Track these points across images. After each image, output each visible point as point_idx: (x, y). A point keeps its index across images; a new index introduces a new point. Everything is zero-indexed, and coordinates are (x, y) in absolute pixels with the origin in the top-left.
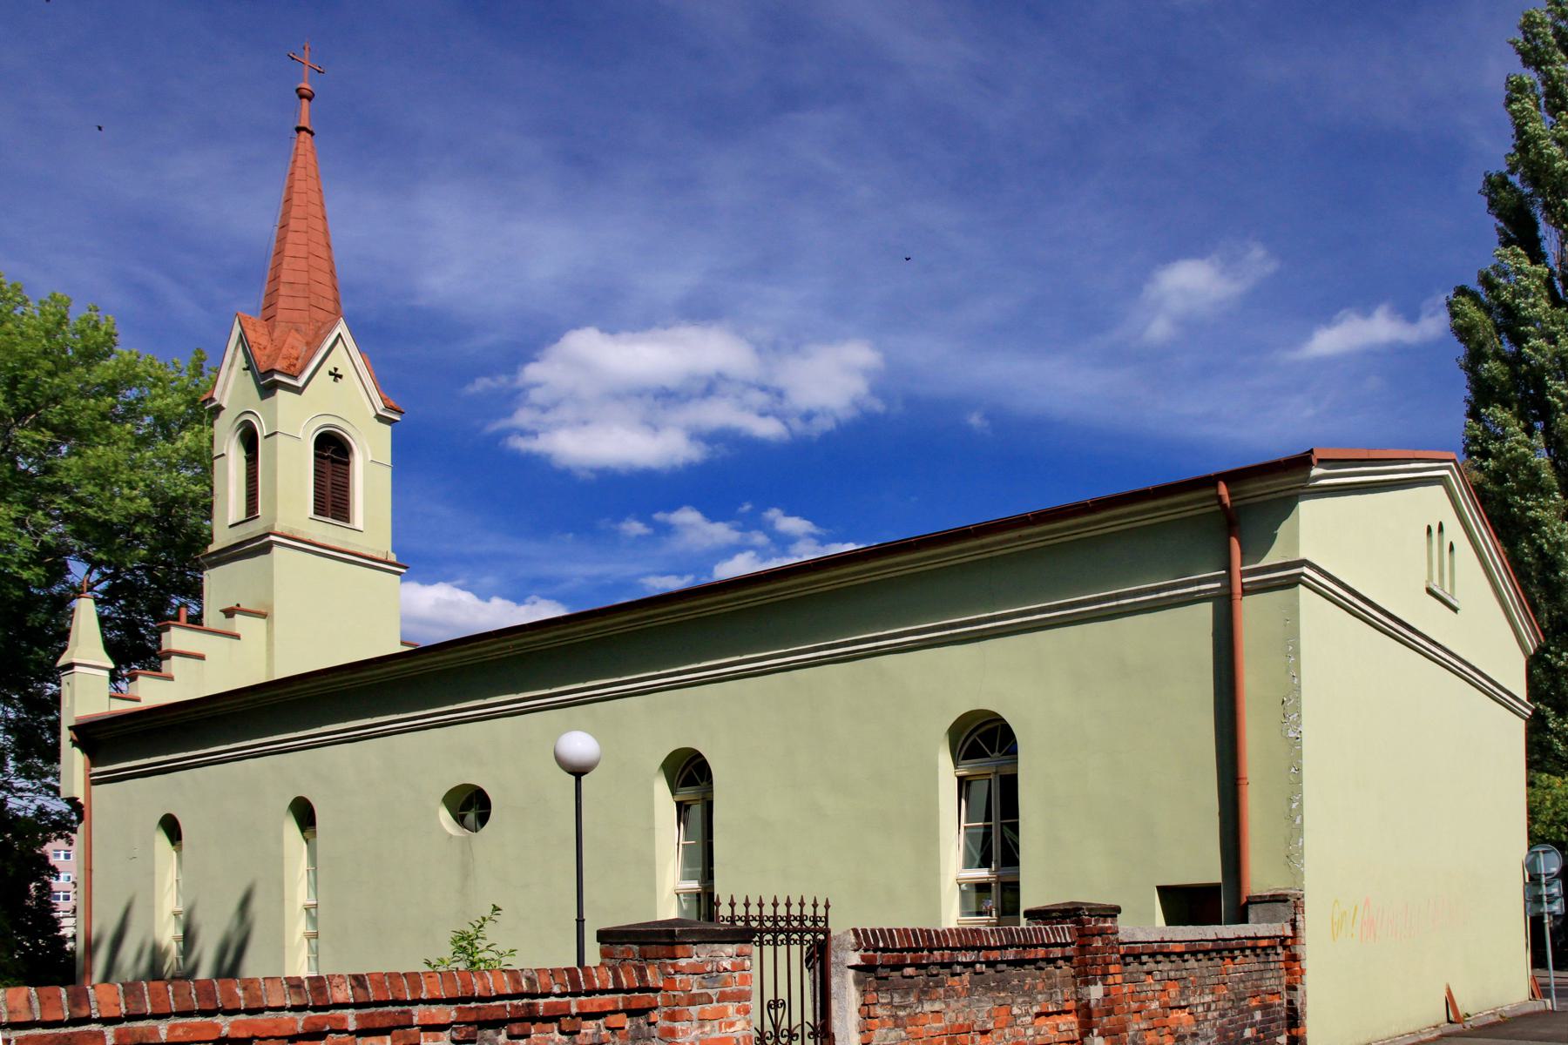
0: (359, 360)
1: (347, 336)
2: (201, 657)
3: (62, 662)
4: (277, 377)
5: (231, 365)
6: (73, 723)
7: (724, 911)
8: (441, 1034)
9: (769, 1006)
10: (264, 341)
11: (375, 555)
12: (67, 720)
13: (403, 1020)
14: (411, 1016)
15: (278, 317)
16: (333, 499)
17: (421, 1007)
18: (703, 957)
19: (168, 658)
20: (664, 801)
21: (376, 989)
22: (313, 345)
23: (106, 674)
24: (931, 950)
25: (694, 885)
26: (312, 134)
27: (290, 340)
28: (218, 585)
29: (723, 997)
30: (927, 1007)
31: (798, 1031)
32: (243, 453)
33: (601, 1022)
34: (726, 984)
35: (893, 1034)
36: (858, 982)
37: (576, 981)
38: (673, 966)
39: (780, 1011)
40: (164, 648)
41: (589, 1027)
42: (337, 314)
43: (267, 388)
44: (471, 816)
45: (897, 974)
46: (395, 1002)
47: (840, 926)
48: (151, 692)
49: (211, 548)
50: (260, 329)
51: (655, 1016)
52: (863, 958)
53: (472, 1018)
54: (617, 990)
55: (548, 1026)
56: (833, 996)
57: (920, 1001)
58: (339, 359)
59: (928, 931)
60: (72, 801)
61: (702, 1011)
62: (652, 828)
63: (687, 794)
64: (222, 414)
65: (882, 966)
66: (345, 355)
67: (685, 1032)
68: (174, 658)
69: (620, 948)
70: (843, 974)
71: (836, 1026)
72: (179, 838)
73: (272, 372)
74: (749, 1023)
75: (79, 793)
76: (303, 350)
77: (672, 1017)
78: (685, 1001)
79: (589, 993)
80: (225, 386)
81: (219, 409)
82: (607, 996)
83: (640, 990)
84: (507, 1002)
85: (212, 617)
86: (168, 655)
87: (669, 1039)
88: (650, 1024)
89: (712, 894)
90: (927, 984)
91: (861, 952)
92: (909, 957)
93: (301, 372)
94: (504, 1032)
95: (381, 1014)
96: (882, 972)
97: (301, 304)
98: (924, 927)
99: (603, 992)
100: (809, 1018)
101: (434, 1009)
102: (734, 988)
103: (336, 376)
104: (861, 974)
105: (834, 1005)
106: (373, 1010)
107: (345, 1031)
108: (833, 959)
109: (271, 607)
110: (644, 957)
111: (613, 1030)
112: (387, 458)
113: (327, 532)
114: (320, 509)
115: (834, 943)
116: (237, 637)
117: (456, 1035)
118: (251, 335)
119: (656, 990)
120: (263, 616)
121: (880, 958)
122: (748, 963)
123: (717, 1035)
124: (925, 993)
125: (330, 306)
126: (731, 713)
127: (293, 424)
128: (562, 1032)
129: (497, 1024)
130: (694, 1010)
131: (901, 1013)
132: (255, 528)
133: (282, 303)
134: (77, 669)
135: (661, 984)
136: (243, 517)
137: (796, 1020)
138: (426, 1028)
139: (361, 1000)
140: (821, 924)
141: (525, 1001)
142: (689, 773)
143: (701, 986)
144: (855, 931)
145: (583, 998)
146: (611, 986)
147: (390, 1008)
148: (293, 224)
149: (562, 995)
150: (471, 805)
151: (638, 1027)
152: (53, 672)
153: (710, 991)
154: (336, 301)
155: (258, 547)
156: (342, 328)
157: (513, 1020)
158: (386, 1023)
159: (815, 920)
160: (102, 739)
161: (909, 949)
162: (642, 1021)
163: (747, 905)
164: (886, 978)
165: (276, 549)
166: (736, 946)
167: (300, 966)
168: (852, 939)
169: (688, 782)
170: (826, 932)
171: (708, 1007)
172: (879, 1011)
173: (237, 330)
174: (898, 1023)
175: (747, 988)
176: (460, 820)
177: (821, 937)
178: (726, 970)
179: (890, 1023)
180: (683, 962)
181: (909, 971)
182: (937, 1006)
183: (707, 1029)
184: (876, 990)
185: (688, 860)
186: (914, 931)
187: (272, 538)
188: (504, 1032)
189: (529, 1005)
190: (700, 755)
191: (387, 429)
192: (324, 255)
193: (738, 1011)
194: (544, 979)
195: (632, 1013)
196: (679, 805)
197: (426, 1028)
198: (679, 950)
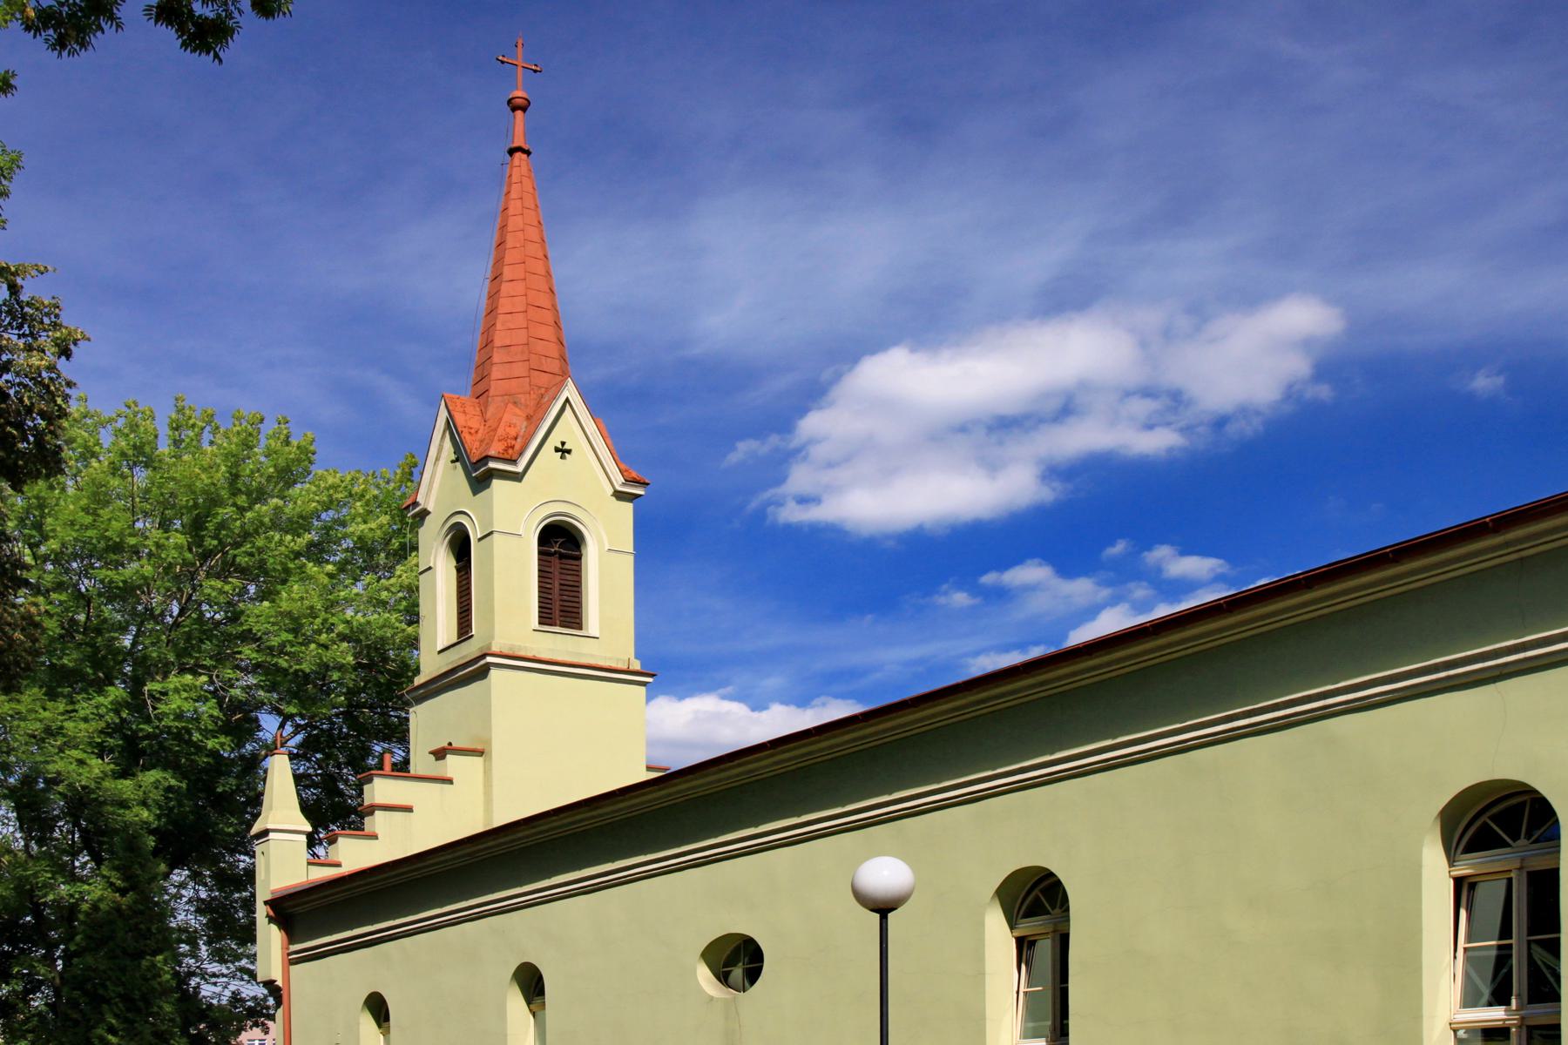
0: (591, 427)
2: (409, 809)
3: (255, 830)
4: (492, 465)
5: (437, 459)
6: (269, 897)
10: (475, 423)
11: (614, 665)
15: (492, 392)
16: (561, 605)
19: (372, 813)
20: (999, 937)
22: (533, 420)
23: (303, 838)
26: (528, 153)
27: (506, 417)
28: (427, 723)
40: (366, 803)
43: (480, 480)
49: (418, 681)
60: (270, 984)
63: (1028, 927)
66: (575, 425)
72: (387, 1019)
73: (486, 458)
75: (277, 976)
76: (522, 425)
85: (420, 761)
86: (372, 809)
93: (521, 453)
97: (520, 369)
103: (563, 451)
109: (489, 742)
113: (556, 644)
114: (546, 618)
116: (450, 781)
118: (460, 419)
125: (554, 366)
127: (511, 519)
132: (469, 650)
133: (496, 373)
134: (272, 835)
142: (1036, 900)
148: (507, 273)
150: (738, 960)
154: (563, 358)
155: (474, 672)
156: (570, 391)
160: (313, 914)
165: (494, 672)
169: (1033, 911)
173: (443, 415)
176: (723, 978)
187: (489, 659)
191: (628, 508)
196: (1020, 942)
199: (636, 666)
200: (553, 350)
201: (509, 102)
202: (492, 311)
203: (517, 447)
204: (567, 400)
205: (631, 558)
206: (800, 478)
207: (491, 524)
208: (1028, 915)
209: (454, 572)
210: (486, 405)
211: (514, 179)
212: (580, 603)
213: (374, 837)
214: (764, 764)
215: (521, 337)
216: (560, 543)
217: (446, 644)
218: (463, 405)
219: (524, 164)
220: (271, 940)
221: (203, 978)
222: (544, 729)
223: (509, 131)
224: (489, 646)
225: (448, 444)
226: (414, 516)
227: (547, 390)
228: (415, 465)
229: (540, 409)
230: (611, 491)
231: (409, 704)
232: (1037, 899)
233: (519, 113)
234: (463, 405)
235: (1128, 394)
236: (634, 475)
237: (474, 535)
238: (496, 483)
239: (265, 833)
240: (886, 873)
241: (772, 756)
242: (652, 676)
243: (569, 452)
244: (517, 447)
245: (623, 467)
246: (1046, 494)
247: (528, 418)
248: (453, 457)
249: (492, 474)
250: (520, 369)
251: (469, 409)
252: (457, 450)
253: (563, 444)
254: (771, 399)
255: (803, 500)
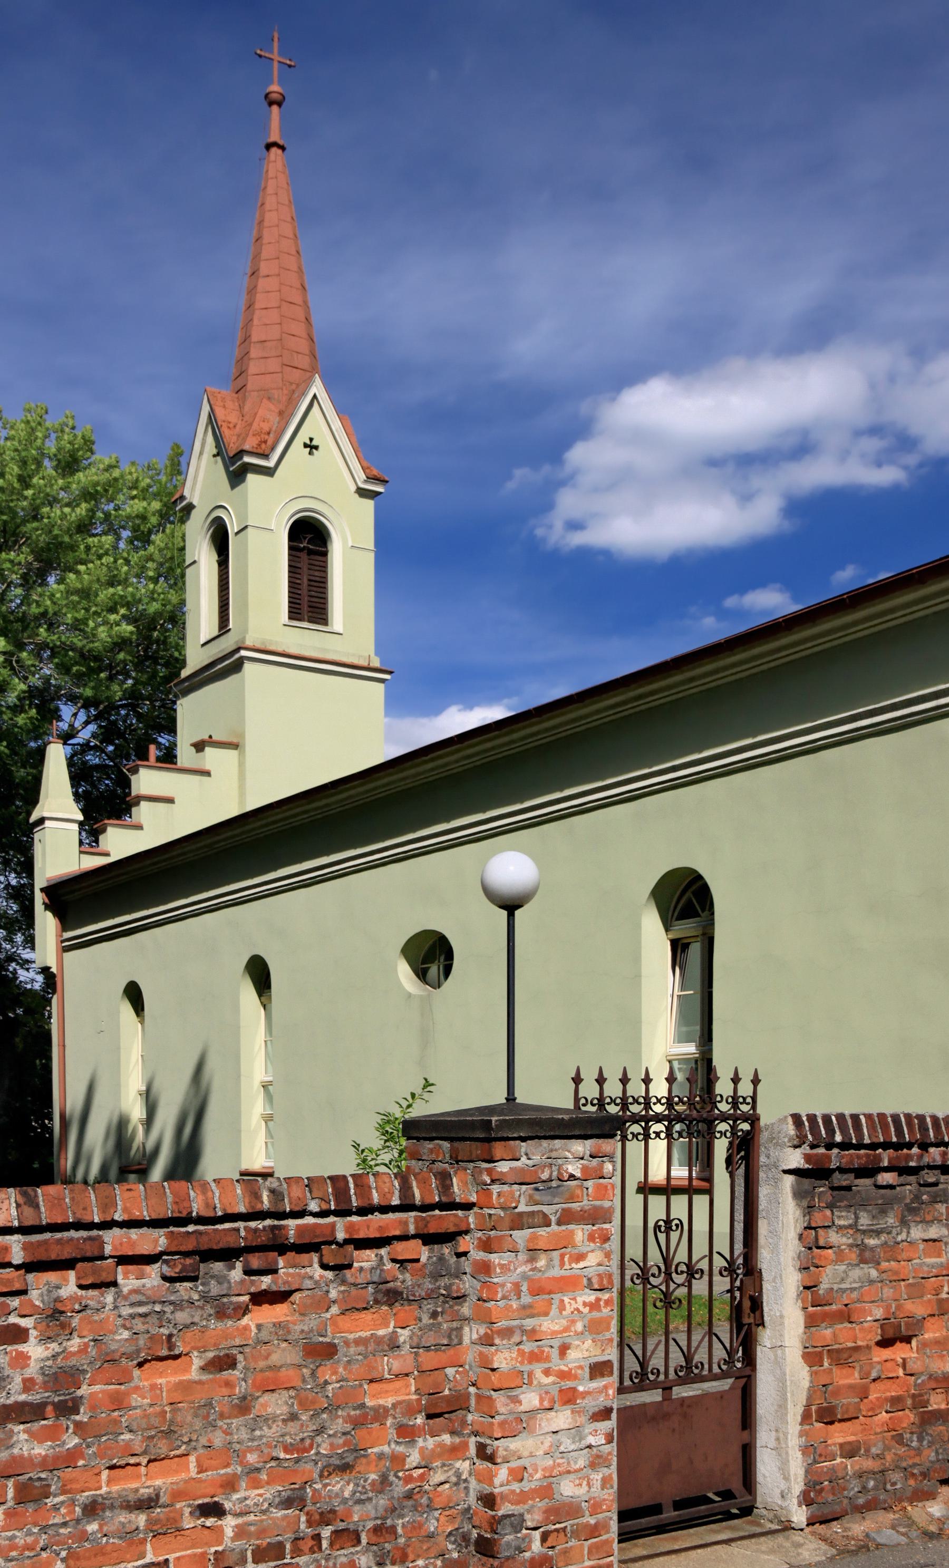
0: (336, 424)
1: (323, 396)
2: (170, 801)
3: (33, 818)
4: (247, 459)
5: (201, 453)
6: (44, 884)
7: (723, 1088)
8: (148, 1269)
9: (657, 1227)
10: (233, 418)
11: (356, 661)
12: (40, 882)
13: (89, 1251)
14: (102, 1244)
15: (249, 387)
16: (309, 600)
17: (116, 1231)
18: (537, 1158)
19: (137, 804)
20: (654, 938)
21: (50, 1209)
22: (285, 415)
23: (75, 827)
24: (924, 1146)
25: (691, 1049)
26: (283, 148)
27: (261, 413)
28: (193, 714)
29: (566, 1218)
30: (917, 1233)
31: (704, 1265)
32: (216, 557)
33: (383, 1251)
34: (572, 1198)
35: (856, 1273)
36: (798, 1194)
37: (342, 1197)
38: (490, 1172)
39: (674, 1236)
40: (133, 794)
41: (366, 1259)
42: (313, 370)
43: (237, 476)
44: (433, 970)
45: (867, 1182)
46: (78, 1225)
47: (773, 1112)
48: (120, 843)
49: (185, 673)
50: (229, 404)
51: (466, 1243)
52: (807, 1158)
53: (189, 1246)
54: (405, 1207)
55: (304, 1258)
56: (762, 1214)
57: (904, 1223)
58: (315, 427)
59: (921, 1118)
60: (45, 970)
61: (534, 1238)
62: (638, 976)
63: (685, 928)
64: (194, 513)
65: (841, 1170)
66: (322, 421)
67: (505, 1268)
68: (143, 803)
69: (429, 1145)
70: (777, 1181)
71: (765, 1258)
72: (143, 1009)
73: (241, 453)
74: (608, 1255)
75: (52, 963)
76: (274, 420)
77: (487, 1246)
78: (507, 1223)
79: (363, 1211)
80: (196, 477)
81: (190, 508)
82: (390, 1216)
83: (442, 1206)
84: (240, 1225)
85: (185, 754)
86: (139, 799)
87: (483, 1278)
88: (459, 1255)
89: (710, 1061)
90: (917, 1198)
91: (806, 1149)
92: (886, 1157)
93: (273, 448)
94: (239, 1265)
95: (59, 1241)
96: (839, 1179)
97: (273, 365)
98: (914, 1110)
99: (385, 1209)
100: (722, 1245)
101: (134, 1234)
102: (586, 1203)
103: (311, 447)
104: (807, 1183)
105: (763, 1228)
106: (47, 1235)
107: (9, 1265)
108: (763, 1159)
109: (242, 735)
110: (456, 1160)
111: (401, 1263)
112: (369, 542)
113: (303, 639)
114: (295, 613)
115: (764, 1137)
116: (207, 773)
117: (166, 1270)
118: (220, 413)
119: (468, 1206)
120: (234, 746)
121: (835, 1158)
122: (608, 1167)
123: (556, 1272)
124: (913, 1212)
125: (304, 362)
126: (721, 817)
127: (264, 514)
128: (324, 1267)
129: (228, 1255)
130: (521, 1236)
131: (872, 1242)
132: (227, 644)
133: (253, 368)
134: (48, 824)
135: (473, 1198)
136: (215, 632)
137: (700, 1248)
138: (123, 1260)
139: (28, 1223)
140: (745, 1108)
141: (268, 1222)
142: (686, 900)
143: (532, 1201)
144: (797, 1118)
145: (355, 1218)
146: (396, 1201)
147: (73, 1234)
148: (264, 268)
149: (323, 1214)
150: (431, 955)
151: (441, 1259)
152: (30, 829)
153: (545, 1209)
154: (313, 355)
155: (227, 666)
156: (317, 388)
157: (249, 1250)
158: (66, 1253)
159: (735, 1101)
160: (87, 901)
161: (886, 1145)
162: (446, 1250)
163: (601, 1081)
164: (848, 1188)
165: (247, 666)
166: (589, 1143)
167: (257, 1160)
168: (791, 1129)
169: (687, 913)
170: (753, 1119)
171: (542, 1232)
172: (834, 1237)
173: (206, 409)
174: (865, 1256)
175: (607, 1204)
176: (421, 974)
177: (745, 1126)
178: (572, 1177)
179: (853, 1256)
180: (503, 1167)
181: (887, 1178)
182: (934, 1232)
183: (541, 1263)
184: (831, 1206)
185: (683, 1017)
186: (896, 1118)
187: (243, 653)
188: (239, 1265)
189: (273, 1228)
190: (699, 877)
191: (369, 504)
192: (298, 299)
193: (591, 1238)
194: (296, 1192)
195: (429, 1239)
196: (675, 944)
197: (123, 1260)
198: (498, 1149)
199: (376, 663)
200: (304, 346)
201: (267, 96)
202: (250, 306)
203: (270, 443)
204: (315, 396)
205: (372, 555)
206: (568, 503)
207: (246, 518)
208: (681, 917)
209: (216, 565)
210: (244, 399)
211: (271, 174)
212: (326, 599)
213: (139, 827)
214: (453, 761)
215: (274, 333)
216: (308, 538)
217: (209, 637)
218: (223, 399)
219: (279, 158)
220: (46, 924)
221: (18, 964)
222: (286, 724)
223: (266, 128)
224: (243, 642)
225: (210, 438)
226: (182, 510)
227: (298, 385)
228: (181, 454)
229: (292, 403)
230: (354, 488)
231: (176, 696)
232: (690, 902)
233: (275, 108)
234: (223, 399)
235: (858, 433)
236: (375, 472)
237: (232, 528)
238: (251, 477)
239: (41, 821)
240: (512, 868)
241: (458, 751)
242: (391, 673)
243: (316, 448)
244: (270, 443)
245: (365, 464)
246: (787, 526)
247: (281, 413)
248: (215, 451)
249: (247, 469)
250: (273, 365)
251: (229, 404)
252: (218, 446)
253: (311, 440)
254: (539, 423)
255: (575, 526)
